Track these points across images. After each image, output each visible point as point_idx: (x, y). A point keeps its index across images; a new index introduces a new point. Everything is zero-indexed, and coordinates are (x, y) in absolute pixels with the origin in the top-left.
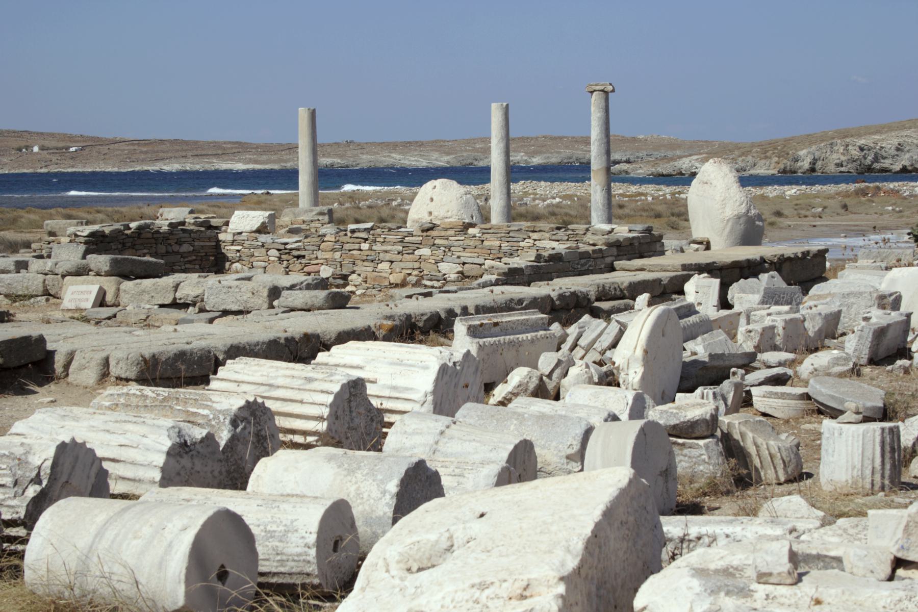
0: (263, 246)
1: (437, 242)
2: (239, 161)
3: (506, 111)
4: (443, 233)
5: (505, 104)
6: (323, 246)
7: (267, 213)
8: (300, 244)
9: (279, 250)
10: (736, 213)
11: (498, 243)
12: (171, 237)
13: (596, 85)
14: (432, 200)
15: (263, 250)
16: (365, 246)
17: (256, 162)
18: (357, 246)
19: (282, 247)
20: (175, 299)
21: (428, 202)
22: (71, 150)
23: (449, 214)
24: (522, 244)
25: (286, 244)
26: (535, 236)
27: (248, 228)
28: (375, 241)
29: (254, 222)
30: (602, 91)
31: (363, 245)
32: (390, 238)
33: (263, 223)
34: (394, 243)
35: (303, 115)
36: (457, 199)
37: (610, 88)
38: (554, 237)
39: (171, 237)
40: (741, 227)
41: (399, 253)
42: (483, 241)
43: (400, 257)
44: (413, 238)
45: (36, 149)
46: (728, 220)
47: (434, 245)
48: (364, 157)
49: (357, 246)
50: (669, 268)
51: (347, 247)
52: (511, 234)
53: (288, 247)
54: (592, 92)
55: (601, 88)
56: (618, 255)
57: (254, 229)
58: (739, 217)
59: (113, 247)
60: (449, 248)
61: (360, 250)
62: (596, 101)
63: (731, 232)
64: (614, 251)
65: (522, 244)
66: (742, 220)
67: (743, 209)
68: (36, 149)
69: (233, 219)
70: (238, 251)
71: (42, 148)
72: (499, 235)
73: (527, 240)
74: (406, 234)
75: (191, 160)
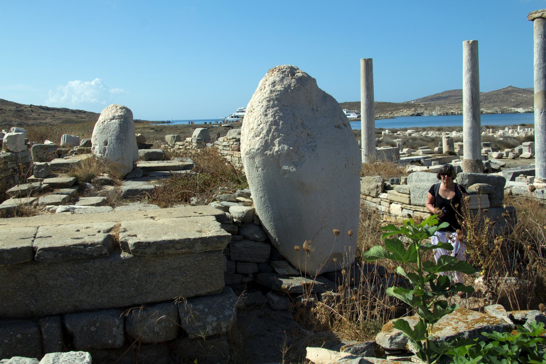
5: (471, 41)
13: (536, 13)
30: (540, 17)
54: (533, 20)
55: (539, 15)
66: (257, 160)
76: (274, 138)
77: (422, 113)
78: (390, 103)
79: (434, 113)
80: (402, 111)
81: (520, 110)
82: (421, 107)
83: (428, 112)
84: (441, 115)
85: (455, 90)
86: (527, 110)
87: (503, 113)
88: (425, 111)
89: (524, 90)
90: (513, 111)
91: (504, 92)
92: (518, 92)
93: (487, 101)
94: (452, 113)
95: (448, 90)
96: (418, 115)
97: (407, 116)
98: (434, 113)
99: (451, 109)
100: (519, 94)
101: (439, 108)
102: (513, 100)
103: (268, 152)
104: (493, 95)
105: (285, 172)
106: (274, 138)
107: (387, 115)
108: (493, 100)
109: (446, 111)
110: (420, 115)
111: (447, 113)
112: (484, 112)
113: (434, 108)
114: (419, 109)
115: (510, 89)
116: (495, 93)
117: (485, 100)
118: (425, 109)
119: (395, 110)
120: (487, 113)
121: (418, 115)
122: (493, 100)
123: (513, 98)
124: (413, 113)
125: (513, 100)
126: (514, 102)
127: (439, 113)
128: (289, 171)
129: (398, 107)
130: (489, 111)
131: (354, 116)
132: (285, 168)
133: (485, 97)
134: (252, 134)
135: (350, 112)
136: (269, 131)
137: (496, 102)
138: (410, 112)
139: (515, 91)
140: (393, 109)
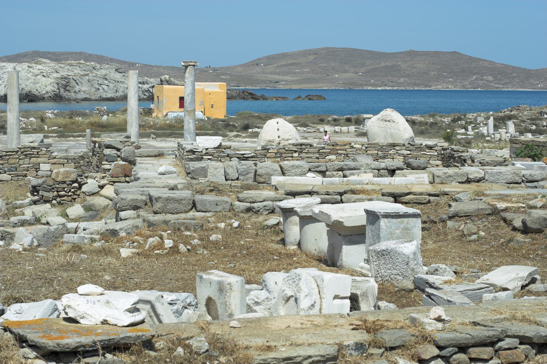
0: (228, 156)
1: (339, 152)
4: (343, 148)
6: (268, 155)
7: (11, 247)
9: (238, 158)
11: (376, 152)
18: (291, 155)
19: (242, 156)
20: (341, 196)
23: (291, 137)
24: (390, 152)
25: (243, 154)
26: (397, 148)
27: (212, 146)
32: (311, 150)
34: (314, 153)
38: (408, 149)
43: (317, 160)
47: (338, 153)
49: (291, 155)
51: (284, 155)
52: (384, 148)
55: (193, 64)
57: (216, 146)
60: (347, 155)
65: (390, 152)
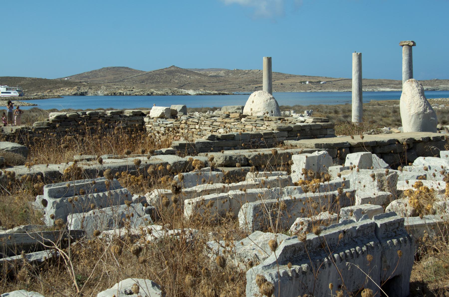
0: (159, 125)
2: (388, 87)
3: (360, 57)
5: (359, 53)
8: (172, 125)
9: (165, 127)
10: (417, 111)
12: (111, 119)
13: (404, 42)
14: (253, 102)
15: (159, 127)
16: (197, 127)
17: (395, 88)
21: (251, 103)
22: (321, 83)
23: (259, 110)
28: (201, 124)
29: (159, 112)
30: (408, 45)
31: (196, 126)
33: (163, 113)
35: (265, 61)
36: (264, 102)
37: (412, 44)
39: (111, 119)
40: (420, 121)
41: (210, 131)
42: (245, 125)
44: (217, 123)
45: (307, 83)
46: (412, 116)
48: (442, 86)
50: (309, 146)
52: (257, 122)
53: (168, 126)
54: (403, 46)
55: (407, 43)
56: (288, 137)
57: (159, 116)
58: (418, 114)
59: (72, 124)
61: (195, 129)
62: (405, 50)
63: (415, 122)
64: (286, 134)
66: (420, 116)
67: (421, 109)
68: (307, 83)
69: (151, 111)
70: (151, 127)
71: (310, 82)
72: (252, 122)
73: (264, 126)
74: (213, 121)
75: (368, 87)
76: (427, 108)
77: (86, 93)
78: (45, 79)
79: (99, 92)
80: (63, 90)
81: (191, 92)
82: (85, 86)
83: (92, 91)
84: (108, 95)
85: (114, 68)
86: (198, 92)
87: (173, 94)
88: (90, 90)
89: (187, 71)
90: (183, 93)
91: (167, 72)
92: (181, 73)
93: (149, 81)
94: (120, 93)
95: (106, 66)
96: (82, 94)
97: (69, 95)
98: (99, 92)
99: (119, 89)
100: (182, 75)
101: (105, 88)
102: (176, 81)
103: (426, 113)
104: (156, 74)
105: (431, 120)
106: (427, 108)
107: (46, 93)
108: (155, 80)
109: (113, 91)
110: (83, 95)
111: (115, 93)
112: (154, 94)
113: (100, 87)
114: (82, 88)
115: (173, 69)
116: (158, 72)
117: (147, 79)
118: (90, 88)
119: (54, 88)
120: (157, 95)
121: (82, 94)
122: (155, 80)
123: (176, 79)
124: (76, 92)
125: (176, 81)
126: (177, 83)
127: (106, 93)
128: (433, 120)
129: (57, 85)
130: (159, 93)
131: (15, 95)
132: (432, 118)
133: (147, 77)
134: (418, 106)
135: (10, 89)
136: (425, 105)
137: (159, 82)
138: (73, 91)
139: (178, 71)
140: (51, 86)
